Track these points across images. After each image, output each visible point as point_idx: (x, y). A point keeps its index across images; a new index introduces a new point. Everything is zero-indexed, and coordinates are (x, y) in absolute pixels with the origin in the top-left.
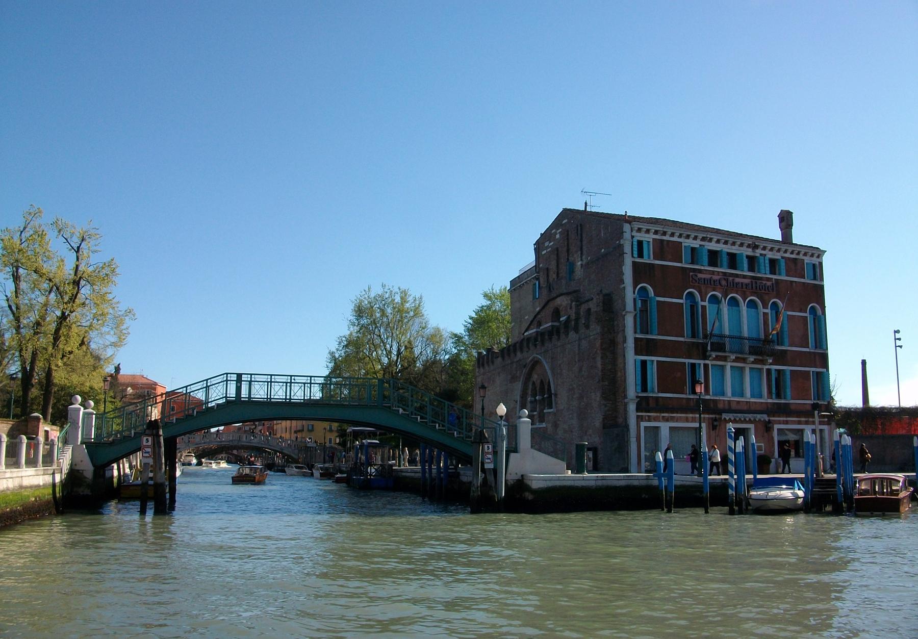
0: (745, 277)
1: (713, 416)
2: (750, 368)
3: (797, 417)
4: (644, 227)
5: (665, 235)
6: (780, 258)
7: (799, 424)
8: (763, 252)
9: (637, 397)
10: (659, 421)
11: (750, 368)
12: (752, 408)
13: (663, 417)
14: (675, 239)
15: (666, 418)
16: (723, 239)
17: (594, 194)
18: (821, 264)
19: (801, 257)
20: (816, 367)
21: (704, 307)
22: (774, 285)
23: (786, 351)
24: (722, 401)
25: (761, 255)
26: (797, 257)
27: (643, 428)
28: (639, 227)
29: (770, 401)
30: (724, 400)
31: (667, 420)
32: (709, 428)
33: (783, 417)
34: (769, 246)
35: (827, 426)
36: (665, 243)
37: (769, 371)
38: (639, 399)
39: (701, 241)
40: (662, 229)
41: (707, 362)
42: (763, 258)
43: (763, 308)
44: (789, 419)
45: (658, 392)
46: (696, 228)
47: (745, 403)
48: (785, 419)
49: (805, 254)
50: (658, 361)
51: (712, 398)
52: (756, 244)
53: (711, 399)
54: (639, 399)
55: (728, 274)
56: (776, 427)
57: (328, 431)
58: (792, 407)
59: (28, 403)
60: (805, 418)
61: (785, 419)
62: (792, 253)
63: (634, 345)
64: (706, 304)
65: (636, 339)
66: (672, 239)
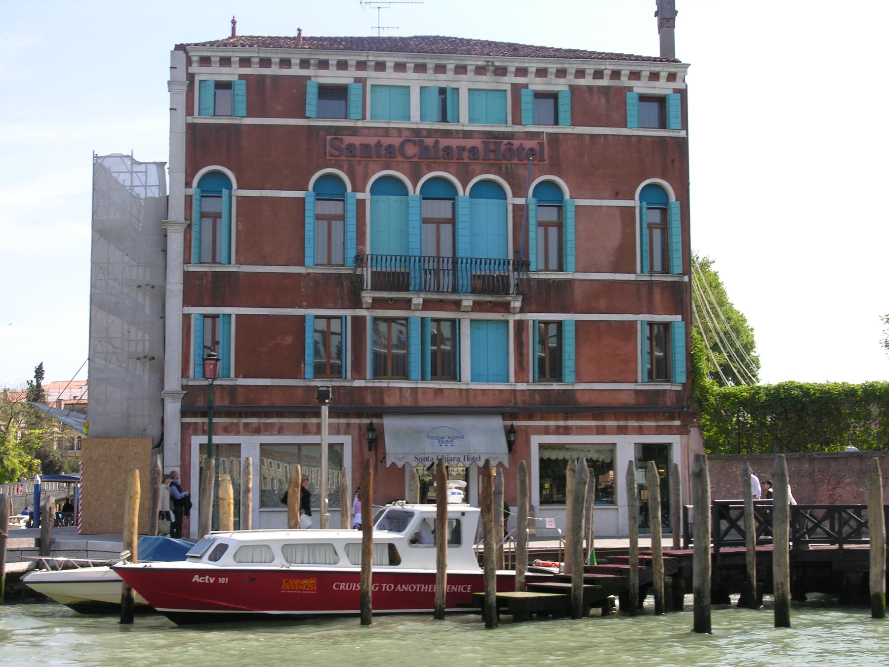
0: (467, 134)
1: (366, 421)
2: (472, 320)
3: (594, 419)
4: (553, 66)
5: (584, 77)
6: (670, 92)
7: (598, 433)
8: (361, 74)
9: (184, 387)
10: (238, 433)
11: (472, 320)
12: (474, 403)
13: (246, 424)
14: (295, 71)
15: (254, 426)
16: (411, 61)
17: (387, 5)
18: (683, 94)
19: (625, 81)
20: (650, 312)
21: (361, 204)
22: (546, 147)
23: (569, 282)
24: (398, 392)
25: (357, 80)
26: (615, 83)
27: (198, 447)
28: (597, 67)
29: (521, 386)
30: (401, 388)
31: (257, 431)
32: (361, 445)
33: (556, 419)
34: (236, 55)
35: (678, 437)
36: (268, 82)
37: (520, 326)
38: (185, 392)
39: (516, 76)
40: (256, 55)
41: (359, 312)
42: (360, 85)
43: (515, 195)
44: (570, 423)
45: (237, 376)
46: (526, 51)
47: (457, 393)
48: (561, 423)
49: (635, 75)
50: (237, 316)
51: (370, 384)
52: (497, 64)
53: (366, 388)
54: (185, 392)
55: (425, 133)
56: (536, 440)
57: (57, 522)
58: (582, 399)
59: (301, 580)
60: (616, 419)
61: (561, 423)
62: (598, 74)
63: (182, 286)
64: (365, 195)
65: (187, 276)
66: (286, 72)
